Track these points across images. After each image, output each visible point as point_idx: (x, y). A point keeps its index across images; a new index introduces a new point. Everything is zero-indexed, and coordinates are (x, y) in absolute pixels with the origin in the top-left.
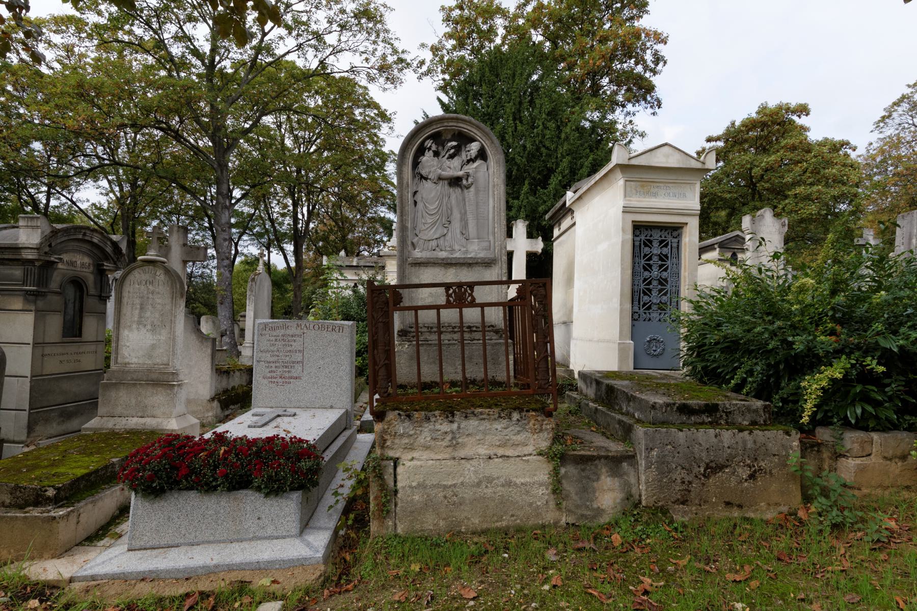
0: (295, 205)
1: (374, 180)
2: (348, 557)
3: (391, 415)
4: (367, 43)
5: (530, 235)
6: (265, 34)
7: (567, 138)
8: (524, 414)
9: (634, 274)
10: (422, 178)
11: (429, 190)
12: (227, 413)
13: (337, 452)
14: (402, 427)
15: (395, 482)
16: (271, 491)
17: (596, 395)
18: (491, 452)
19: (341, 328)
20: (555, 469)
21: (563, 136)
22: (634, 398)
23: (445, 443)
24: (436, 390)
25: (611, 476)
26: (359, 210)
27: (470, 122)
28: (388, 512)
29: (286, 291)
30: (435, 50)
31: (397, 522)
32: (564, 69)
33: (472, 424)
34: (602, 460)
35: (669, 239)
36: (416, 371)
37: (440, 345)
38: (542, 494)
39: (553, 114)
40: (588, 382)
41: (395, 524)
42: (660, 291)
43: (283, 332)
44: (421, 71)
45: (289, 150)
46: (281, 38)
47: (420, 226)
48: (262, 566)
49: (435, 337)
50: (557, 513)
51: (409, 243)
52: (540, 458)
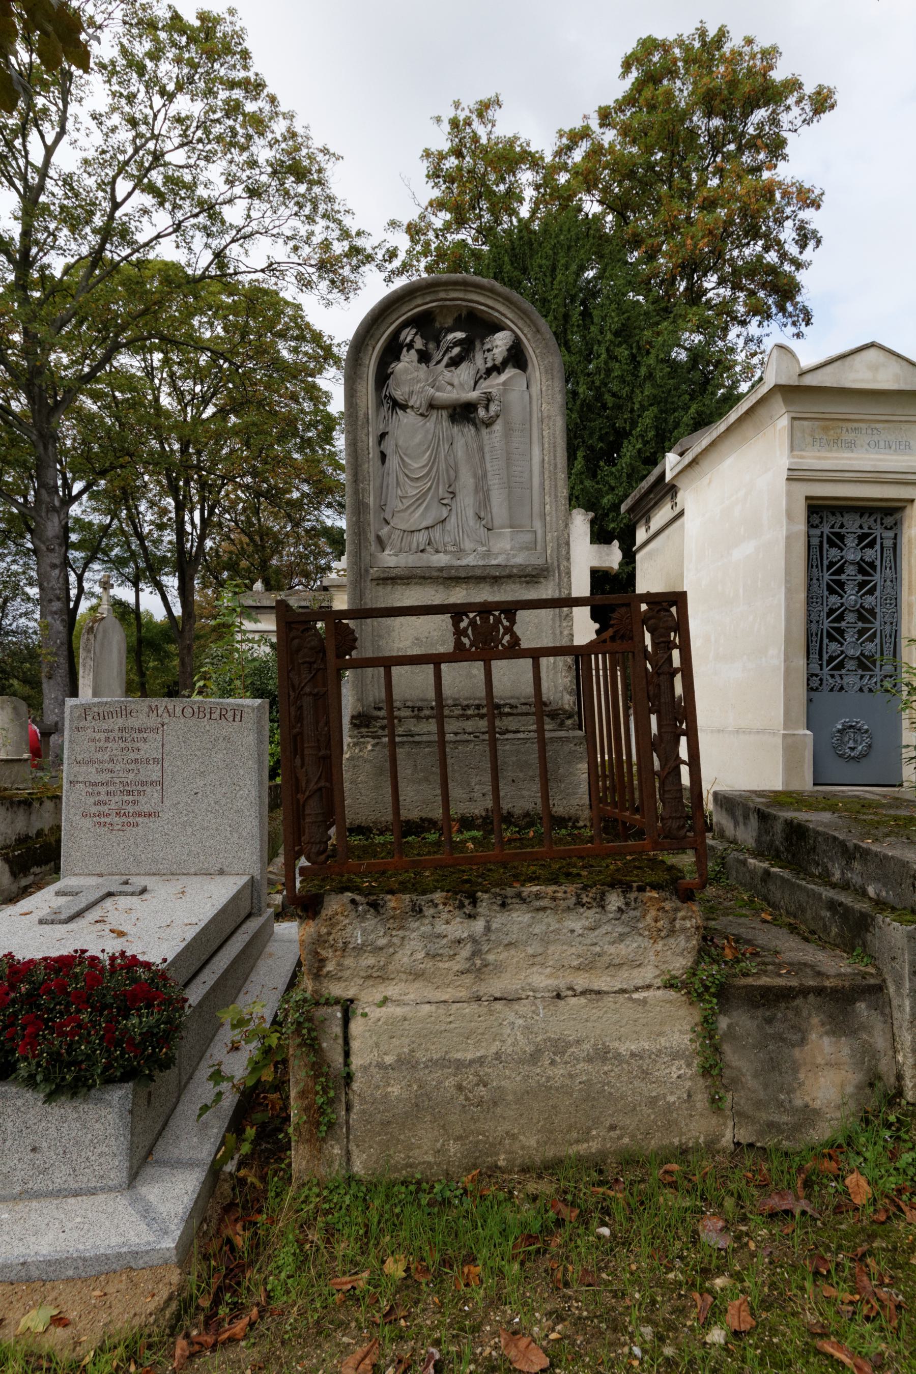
0: (180, 508)
1: (314, 462)
2: (241, 1240)
3: (335, 904)
4: (295, 222)
6: (116, 206)
7: (650, 376)
8: (632, 896)
9: (811, 600)
10: (398, 405)
11: (409, 429)
12: (24, 882)
13: (227, 971)
14: (357, 932)
15: (347, 1054)
16: (58, 1086)
17: (758, 840)
18: (562, 983)
19: (238, 713)
20: (706, 1020)
21: (643, 371)
22: (865, 854)
23: (457, 965)
24: (432, 837)
25: (832, 1033)
26: (289, 516)
27: (492, 290)
28: (331, 1125)
29: (168, 655)
30: (414, 231)
31: (353, 1147)
32: (639, 261)
33: (518, 919)
34: (811, 997)
35: (878, 531)
36: (389, 798)
37: (442, 743)
38: (678, 1077)
39: (624, 333)
40: (739, 813)
41: (348, 1153)
42: (861, 633)
43: (120, 722)
44: (390, 267)
45: (168, 414)
46: (145, 211)
47: (394, 503)
48: (35, 1273)
49: (432, 726)
50: (714, 1121)
51: (372, 538)
52: (672, 994)
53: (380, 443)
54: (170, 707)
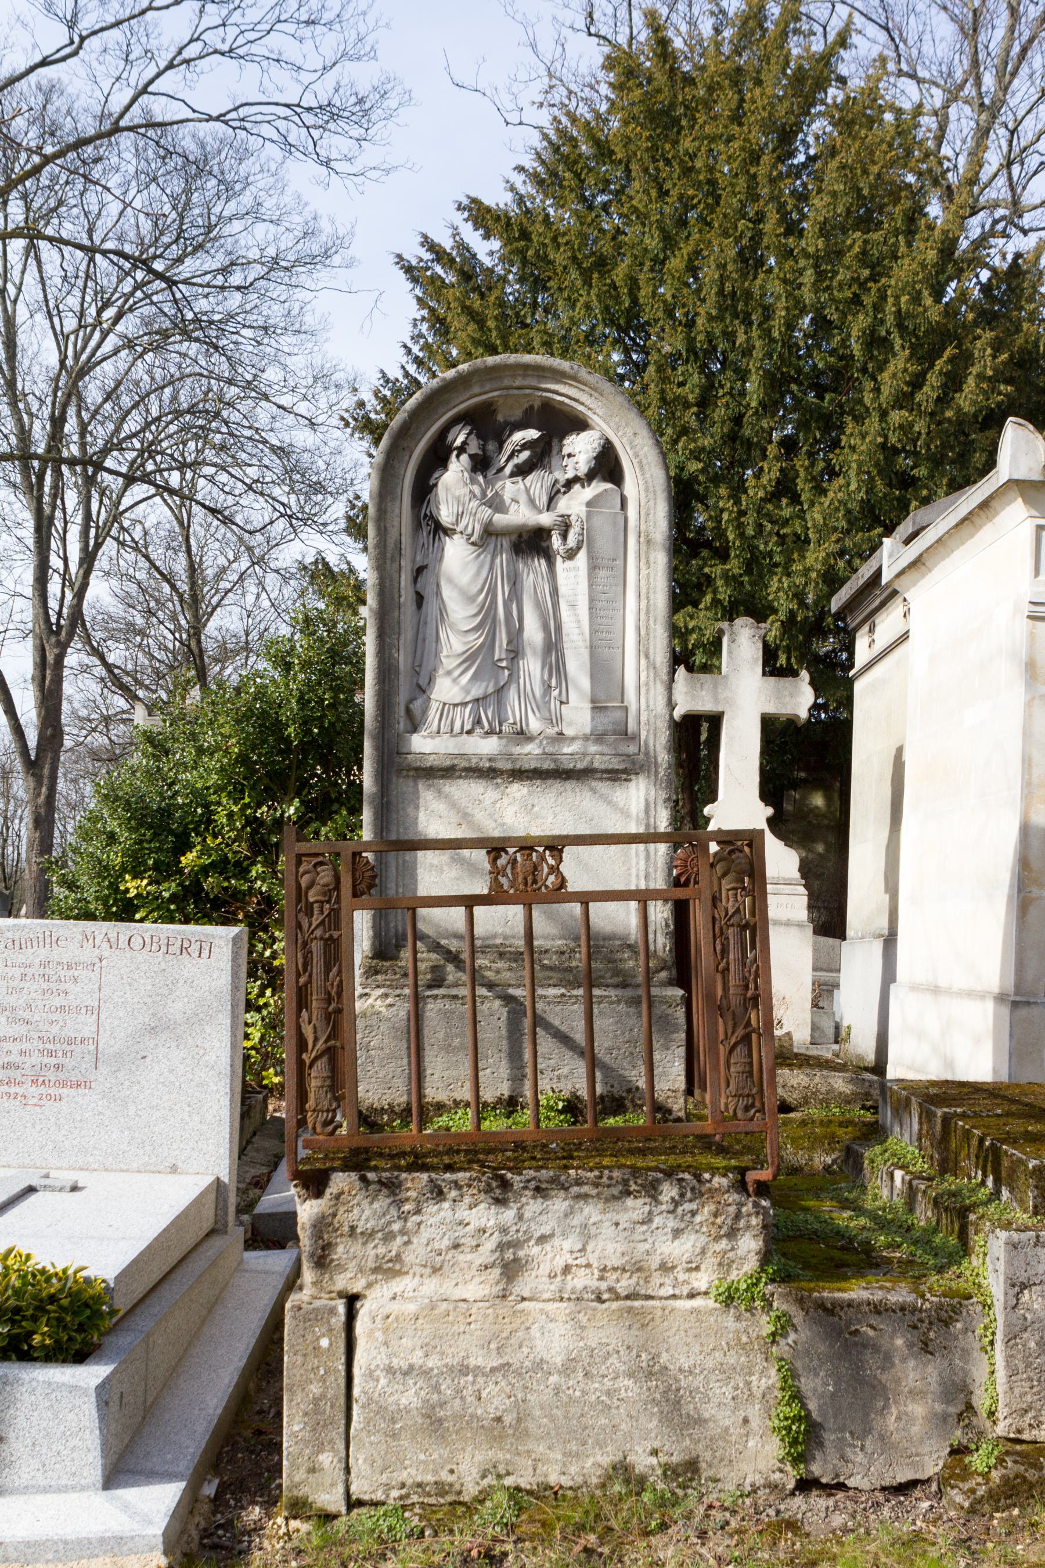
5: (773, 665)
13: (592, 600)
43: (43, 953)
53: (415, 580)
54: (112, 936)
